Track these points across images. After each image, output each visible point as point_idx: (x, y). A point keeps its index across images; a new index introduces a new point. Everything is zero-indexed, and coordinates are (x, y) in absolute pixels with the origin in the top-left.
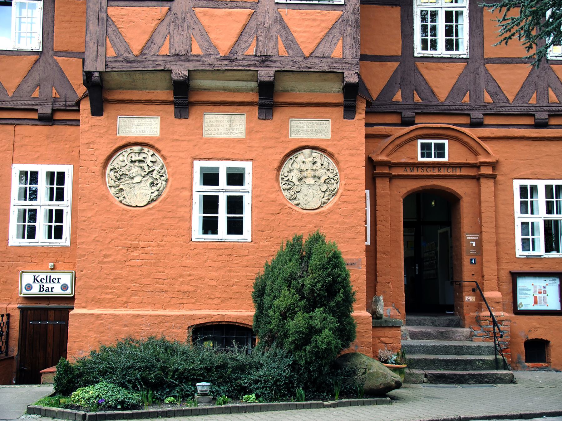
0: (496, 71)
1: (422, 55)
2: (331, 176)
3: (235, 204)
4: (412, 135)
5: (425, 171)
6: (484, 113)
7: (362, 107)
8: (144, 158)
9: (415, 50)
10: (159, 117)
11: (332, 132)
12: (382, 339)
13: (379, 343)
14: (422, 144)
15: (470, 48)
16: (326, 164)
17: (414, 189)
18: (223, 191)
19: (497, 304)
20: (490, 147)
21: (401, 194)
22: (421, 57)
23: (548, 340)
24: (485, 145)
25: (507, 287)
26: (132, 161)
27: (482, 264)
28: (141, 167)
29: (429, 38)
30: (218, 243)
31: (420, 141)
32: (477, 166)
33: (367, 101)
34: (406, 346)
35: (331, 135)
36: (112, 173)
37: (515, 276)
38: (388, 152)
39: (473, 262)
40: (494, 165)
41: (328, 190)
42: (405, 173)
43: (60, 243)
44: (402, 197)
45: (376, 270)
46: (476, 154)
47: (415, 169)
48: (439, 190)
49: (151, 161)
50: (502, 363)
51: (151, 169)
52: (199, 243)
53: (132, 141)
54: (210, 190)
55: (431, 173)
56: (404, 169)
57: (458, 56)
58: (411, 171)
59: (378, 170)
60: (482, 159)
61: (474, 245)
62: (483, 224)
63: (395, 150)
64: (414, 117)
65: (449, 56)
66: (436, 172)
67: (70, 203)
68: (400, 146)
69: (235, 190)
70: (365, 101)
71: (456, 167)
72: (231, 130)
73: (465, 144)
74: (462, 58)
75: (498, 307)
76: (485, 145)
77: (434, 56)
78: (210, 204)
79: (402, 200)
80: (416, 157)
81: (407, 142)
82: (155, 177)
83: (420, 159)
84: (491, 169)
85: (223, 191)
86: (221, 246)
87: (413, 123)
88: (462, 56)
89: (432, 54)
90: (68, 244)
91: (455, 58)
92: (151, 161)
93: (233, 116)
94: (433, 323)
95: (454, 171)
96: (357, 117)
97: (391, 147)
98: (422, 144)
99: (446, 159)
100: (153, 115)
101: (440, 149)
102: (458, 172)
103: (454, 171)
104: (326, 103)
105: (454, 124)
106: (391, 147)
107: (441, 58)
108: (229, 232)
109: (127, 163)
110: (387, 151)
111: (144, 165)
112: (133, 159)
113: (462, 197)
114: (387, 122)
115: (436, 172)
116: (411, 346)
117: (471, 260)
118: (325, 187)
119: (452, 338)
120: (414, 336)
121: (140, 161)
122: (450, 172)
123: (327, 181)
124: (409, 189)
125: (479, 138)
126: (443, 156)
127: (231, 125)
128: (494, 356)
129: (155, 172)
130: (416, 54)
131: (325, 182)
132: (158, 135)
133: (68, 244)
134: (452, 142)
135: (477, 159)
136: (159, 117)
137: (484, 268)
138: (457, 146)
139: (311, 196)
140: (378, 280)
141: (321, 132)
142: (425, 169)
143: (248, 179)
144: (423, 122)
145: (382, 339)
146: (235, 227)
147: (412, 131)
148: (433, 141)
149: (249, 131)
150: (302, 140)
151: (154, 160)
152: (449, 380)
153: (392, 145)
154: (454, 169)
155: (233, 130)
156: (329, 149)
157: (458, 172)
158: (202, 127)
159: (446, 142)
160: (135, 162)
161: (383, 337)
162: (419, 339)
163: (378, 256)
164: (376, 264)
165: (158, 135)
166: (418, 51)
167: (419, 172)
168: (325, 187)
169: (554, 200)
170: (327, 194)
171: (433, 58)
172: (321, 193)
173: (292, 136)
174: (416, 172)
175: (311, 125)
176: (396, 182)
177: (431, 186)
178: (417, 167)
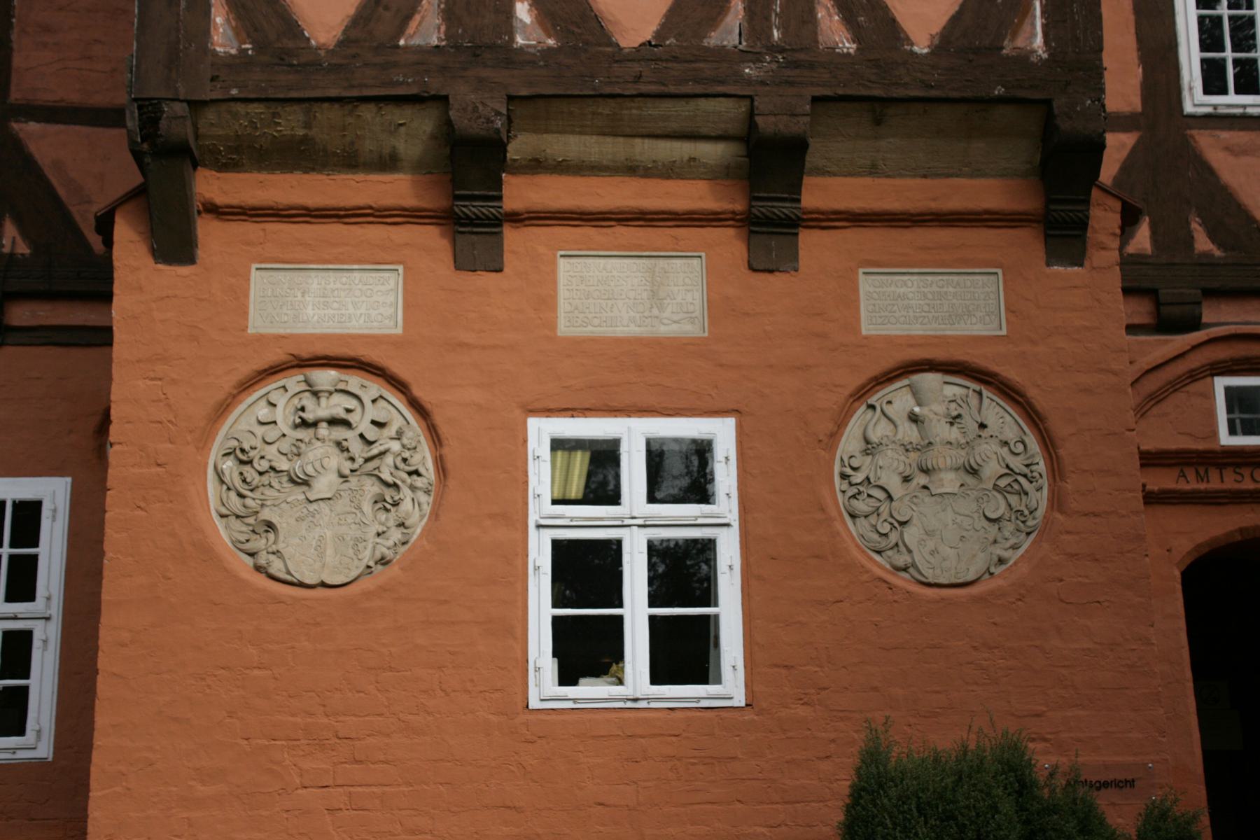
1: (1209, 110)
3: (681, 570)
4: (1195, 361)
8: (348, 411)
10: (401, 268)
14: (1228, 390)
18: (637, 524)
22: (1207, 116)
26: (304, 424)
28: (338, 444)
29: (1229, 54)
30: (627, 715)
31: (1221, 384)
33: (1124, 203)
36: (229, 465)
43: (14, 750)
47: (1214, 474)
49: (374, 422)
51: (375, 450)
52: (554, 717)
53: (305, 353)
54: (589, 522)
56: (1175, 472)
58: (1200, 479)
64: (1199, 303)
67: (56, 610)
69: (681, 520)
70: (1117, 205)
72: (655, 312)
77: (1250, 111)
78: (586, 571)
79: (1177, 573)
80: (1214, 434)
81: (1175, 386)
82: (390, 479)
83: (1226, 439)
85: (637, 524)
86: (631, 719)
87: (1194, 324)
89: (1244, 106)
90: (45, 750)
92: (374, 422)
93: (661, 262)
98: (1228, 390)
100: (375, 259)
104: (987, 212)
108: (659, 675)
109: (287, 430)
111: (350, 436)
112: (309, 416)
121: (334, 422)
124: (1201, 538)
127: (654, 294)
129: (389, 459)
130: (1189, 108)
132: (399, 331)
133: (45, 750)
136: (401, 268)
139: (949, 537)
142: (1246, 472)
143: (725, 477)
144: (1223, 317)
146: (683, 652)
147: (1194, 348)
149: (718, 308)
150: (911, 341)
151: (370, 437)
155: (661, 308)
156: (1011, 373)
158: (548, 302)
160: (315, 424)
165: (399, 331)
166: (1195, 100)
167: (1229, 481)
170: (1009, 528)
171: (1244, 117)
173: (259, 322)
174: (1215, 482)
175: (935, 288)
178: (1221, 467)
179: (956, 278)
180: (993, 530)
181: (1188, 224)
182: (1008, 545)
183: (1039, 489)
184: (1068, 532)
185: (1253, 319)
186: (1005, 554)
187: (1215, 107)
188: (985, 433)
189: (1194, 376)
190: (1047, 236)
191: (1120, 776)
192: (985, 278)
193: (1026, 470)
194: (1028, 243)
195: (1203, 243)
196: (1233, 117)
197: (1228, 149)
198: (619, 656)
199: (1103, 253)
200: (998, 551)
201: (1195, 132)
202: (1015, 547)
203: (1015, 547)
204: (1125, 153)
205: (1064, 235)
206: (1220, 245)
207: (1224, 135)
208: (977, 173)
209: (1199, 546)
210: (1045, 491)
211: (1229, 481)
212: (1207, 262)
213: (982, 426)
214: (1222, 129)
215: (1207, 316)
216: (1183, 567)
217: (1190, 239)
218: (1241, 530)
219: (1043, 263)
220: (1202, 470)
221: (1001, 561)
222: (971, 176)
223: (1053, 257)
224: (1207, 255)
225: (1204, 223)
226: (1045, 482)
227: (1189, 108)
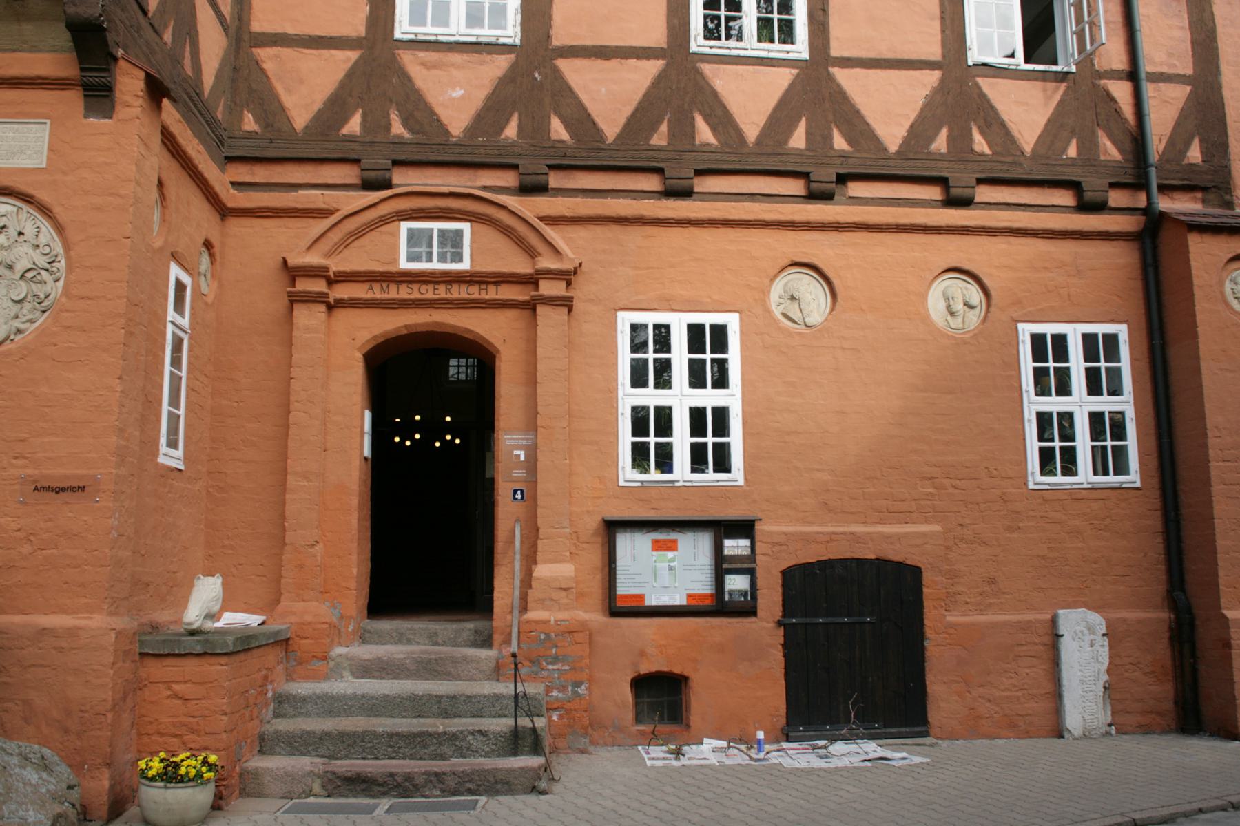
0: (575, 72)
1: (412, 37)
2: (42, 262)
4: (384, 209)
5: (416, 290)
6: (549, 162)
7: (129, 84)
9: (397, 25)
11: (50, 150)
12: (176, 687)
13: (169, 697)
15: (522, 24)
16: (29, 230)
17: (386, 333)
19: (564, 593)
20: (563, 238)
21: (359, 343)
23: (686, 674)
24: (549, 232)
25: (594, 556)
27: (535, 499)
31: (405, 226)
32: (532, 281)
33: (147, 73)
34: (318, 698)
35: (48, 158)
37: (612, 527)
38: (327, 248)
39: (519, 496)
40: (567, 277)
41: (30, 298)
42: (369, 296)
44: (359, 349)
45: (283, 517)
46: (532, 253)
47: (393, 287)
48: (481, 346)
50: (529, 740)
55: (430, 295)
56: (367, 286)
57: (493, 40)
59: (303, 285)
60: (547, 262)
61: (522, 458)
62: (539, 409)
63: (345, 243)
65: (473, 39)
66: (441, 292)
68: (358, 234)
70: (142, 75)
71: (487, 283)
73: (506, 231)
74: (504, 45)
75: (565, 601)
76: (549, 232)
77: (441, 38)
79: (359, 356)
80: (396, 261)
84: (564, 284)
87: (387, 185)
88: (502, 41)
91: (488, 44)
94: (430, 637)
95: (483, 292)
96: (121, 112)
97: (335, 236)
99: (465, 265)
101: (452, 242)
102: (492, 293)
103: (483, 292)
104: (39, 78)
105: (485, 188)
106: (335, 236)
107: (457, 43)
110: (325, 245)
113: (498, 351)
114: (330, 181)
115: (441, 292)
116: (333, 697)
117: (515, 492)
118: (22, 289)
119: (449, 674)
120: (365, 670)
122: (474, 292)
123: (30, 275)
125: (541, 219)
126: (458, 258)
128: (511, 722)
130: (398, 35)
131: (22, 277)
134: (478, 226)
135: (534, 264)
137: (539, 511)
138: (493, 238)
140: (287, 541)
141: (22, 152)
144: (404, 179)
145: (176, 687)
148: (436, 226)
152: (376, 788)
153: (336, 230)
154: (483, 287)
156: (42, 195)
157: (492, 293)
159: (465, 227)
161: (177, 682)
162: (374, 677)
163: (291, 481)
164: (283, 503)
167: (404, 293)
168: (22, 289)
169: (708, 356)
170: (27, 306)
171: (437, 43)
172: (10, 304)
176: (341, 314)
177: (427, 324)
179: (16, 126)
180: (16, 308)
181: (388, 115)
182: (24, 319)
183: (57, 280)
184: (67, 311)
185: (429, 182)
186: (22, 326)
187: (416, 35)
188: (22, 238)
189: (384, 221)
190: (85, 96)
191: (76, 484)
192: (37, 126)
193: (48, 266)
194: (74, 98)
195: (398, 128)
196: (430, 42)
197: (423, 64)
198: (663, 472)
199: (127, 109)
200: (17, 324)
201: (400, 52)
202: (31, 321)
203: (31, 321)
204: (349, 65)
205: (98, 95)
206: (411, 130)
207: (421, 54)
208: (34, 49)
209: (375, 337)
210: (61, 284)
211: (404, 293)
212: (399, 143)
213: (20, 234)
214: (421, 50)
215: (395, 181)
216: (365, 351)
217: (388, 127)
218: (406, 326)
219: (81, 116)
220: (385, 285)
221: (19, 331)
222: (30, 51)
223: (90, 111)
224: (400, 136)
225: (401, 115)
226: (62, 274)
227: (398, 35)
